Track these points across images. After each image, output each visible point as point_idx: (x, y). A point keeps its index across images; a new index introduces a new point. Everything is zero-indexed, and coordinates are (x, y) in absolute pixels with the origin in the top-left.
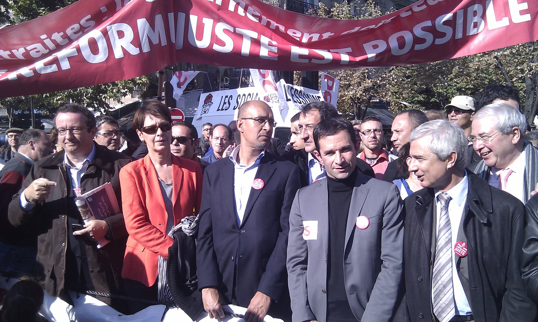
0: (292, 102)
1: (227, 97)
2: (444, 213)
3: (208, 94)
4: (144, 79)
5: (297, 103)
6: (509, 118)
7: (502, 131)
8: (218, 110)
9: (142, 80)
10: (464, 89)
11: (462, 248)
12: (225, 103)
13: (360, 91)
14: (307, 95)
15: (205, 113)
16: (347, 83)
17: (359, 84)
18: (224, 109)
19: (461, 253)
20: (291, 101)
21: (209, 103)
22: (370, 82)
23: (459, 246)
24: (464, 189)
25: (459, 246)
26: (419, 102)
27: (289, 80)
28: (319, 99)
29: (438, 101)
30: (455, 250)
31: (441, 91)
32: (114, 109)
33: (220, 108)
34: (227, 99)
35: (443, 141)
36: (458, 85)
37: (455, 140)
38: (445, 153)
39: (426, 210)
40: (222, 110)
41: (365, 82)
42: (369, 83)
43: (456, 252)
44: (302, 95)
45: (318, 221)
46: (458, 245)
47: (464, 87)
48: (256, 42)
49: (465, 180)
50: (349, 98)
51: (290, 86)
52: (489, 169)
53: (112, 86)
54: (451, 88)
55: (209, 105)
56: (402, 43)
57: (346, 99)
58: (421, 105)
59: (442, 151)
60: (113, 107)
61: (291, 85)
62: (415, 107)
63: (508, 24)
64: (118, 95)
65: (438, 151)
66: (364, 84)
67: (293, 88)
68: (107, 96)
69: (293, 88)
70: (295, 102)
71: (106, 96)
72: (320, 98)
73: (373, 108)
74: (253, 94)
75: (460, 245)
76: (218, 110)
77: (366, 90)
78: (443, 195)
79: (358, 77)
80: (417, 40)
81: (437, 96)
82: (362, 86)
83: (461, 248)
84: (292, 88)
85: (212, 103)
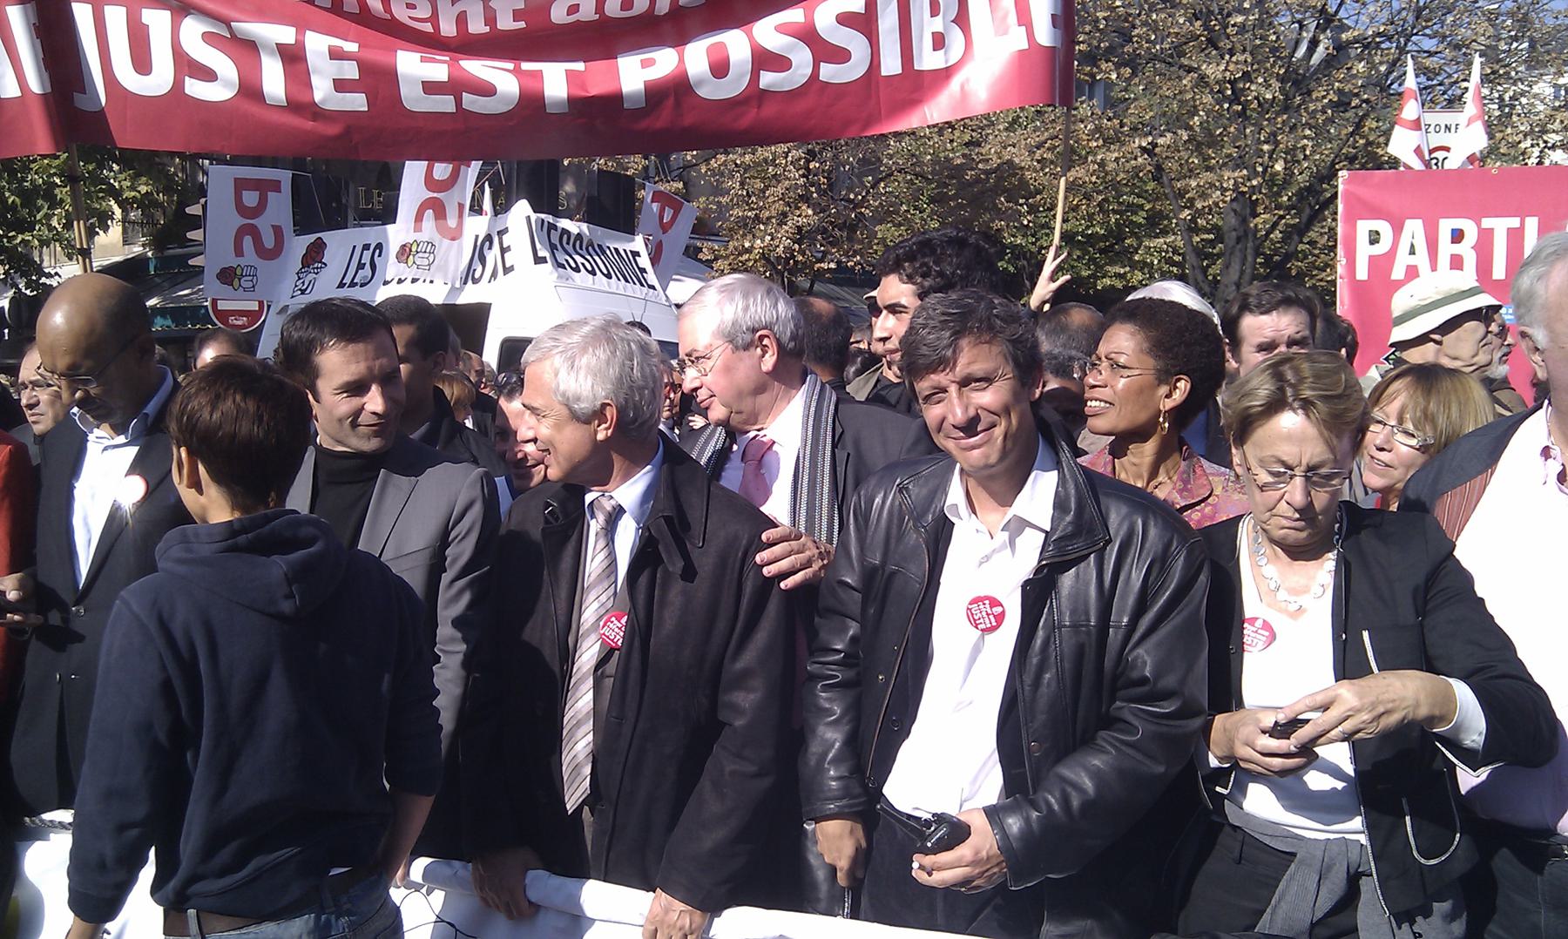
0: (549, 266)
1: (366, 247)
2: (602, 544)
3: (312, 238)
4: (146, 188)
5: (566, 269)
6: (746, 308)
7: (731, 342)
8: (341, 285)
9: (139, 189)
10: (1080, 238)
11: (988, 615)
12: (361, 266)
13: (784, 238)
14: (600, 246)
15: (302, 294)
16: (750, 214)
17: (783, 218)
18: (356, 284)
20: (547, 262)
21: (316, 265)
27: (545, 201)
28: (637, 258)
29: (1011, 269)
30: (970, 607)
31: (1019, 242)
32: (57, 277)
33: (347, 280)
34: (367, 255)
35: (582, 374)
37: (613, 372)
38: (584, 406)
39: (567, 538)
40: (353, 284)
41: (798, 213)
42: (809, 216)
44: (584, 248)
47: (1080, 230)
48: (293, 57)
50: (757, 257)
51: (546, 220)
52: (728, 439)
53: (46, 207)
55: (316, 271)
56: (720, 68)
57: (749, 260)
59: (578, 399)
60: (53, 272)
61: (549, 218)
64: (67, 236)
65: (568, 399)
66: (795, 218)
67: (555, 227)
68: (30, 238)
69: (556, 226)
70: (559, 267)
71: (27, 238)
72: (639, 256)
73: (842, 286)
76: (341, 285)
77: (801, 235)
79: (781, 199)
80: (764, 59)
81: (1009, 255)
82: (789, 223)
84: (552, 227)
85: (326, 265)
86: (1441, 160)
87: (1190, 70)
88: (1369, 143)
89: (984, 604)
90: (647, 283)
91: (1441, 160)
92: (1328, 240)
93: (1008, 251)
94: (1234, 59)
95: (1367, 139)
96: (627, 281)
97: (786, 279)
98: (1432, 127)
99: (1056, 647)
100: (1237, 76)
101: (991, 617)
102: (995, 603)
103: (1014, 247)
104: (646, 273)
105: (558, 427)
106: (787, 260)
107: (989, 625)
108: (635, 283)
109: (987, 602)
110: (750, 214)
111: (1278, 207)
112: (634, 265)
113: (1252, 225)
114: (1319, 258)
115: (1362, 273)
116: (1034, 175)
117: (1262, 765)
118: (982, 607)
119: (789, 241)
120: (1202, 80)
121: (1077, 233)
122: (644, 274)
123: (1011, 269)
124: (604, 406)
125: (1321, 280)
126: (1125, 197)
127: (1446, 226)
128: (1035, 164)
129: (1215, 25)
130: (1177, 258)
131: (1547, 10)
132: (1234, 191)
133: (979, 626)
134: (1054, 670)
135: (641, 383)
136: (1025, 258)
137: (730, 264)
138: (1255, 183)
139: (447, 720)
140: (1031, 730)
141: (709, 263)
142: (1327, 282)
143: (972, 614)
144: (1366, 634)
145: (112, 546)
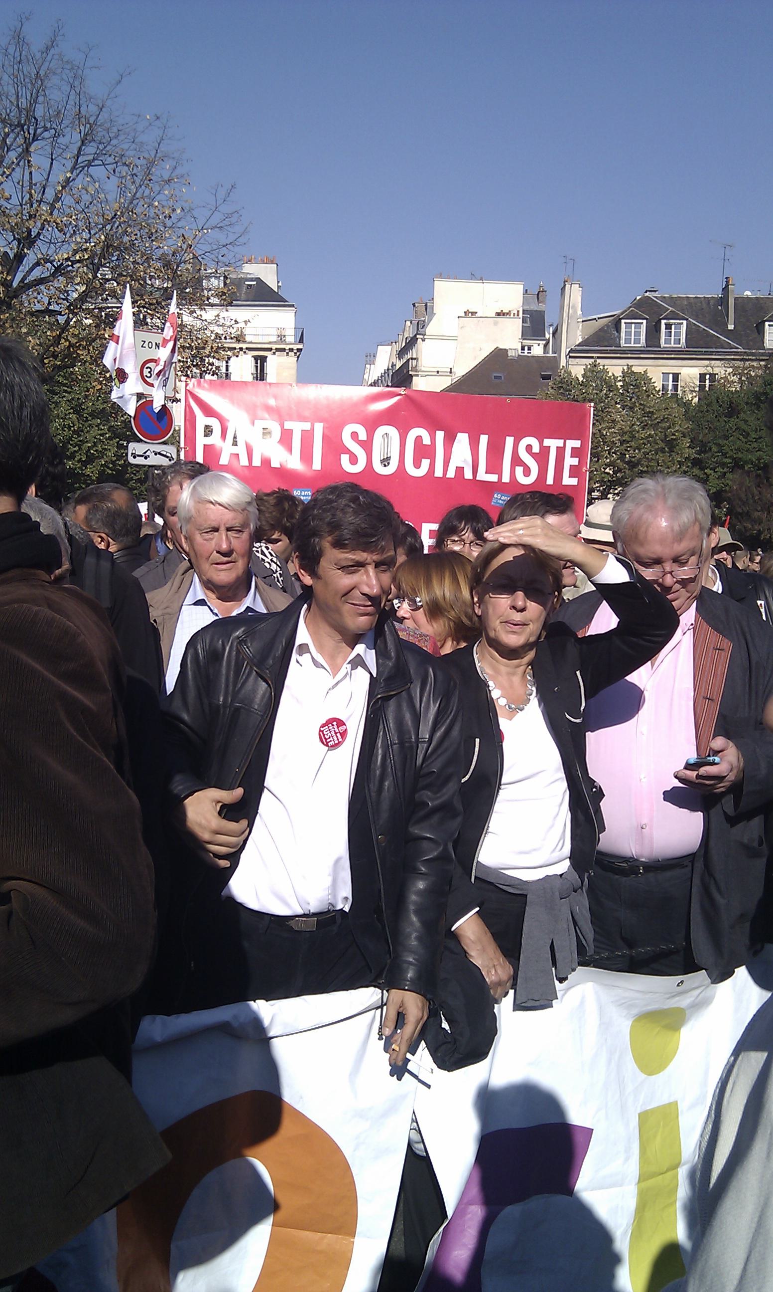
11: (336, 733)
19: (328, 741)
23: (333, 725)
25: (333, 725)
30: (322, 729)
43: (321, 733)
45: (423, 524)
46: (333, 723)
63: (496, 480)
74: (429, 1086)
75: (335, 726)
83: (335, 731)
98: (147, 343)
99: (391, 760)
101: (338, 735)
102: (340, 723)
107: (336, 742)
109: (335, 723)
118: (331, 728)
134: (391, 778)
139: (711, 1185)
140: (377, 827)
143: (324, 735)
145: (540, 772)
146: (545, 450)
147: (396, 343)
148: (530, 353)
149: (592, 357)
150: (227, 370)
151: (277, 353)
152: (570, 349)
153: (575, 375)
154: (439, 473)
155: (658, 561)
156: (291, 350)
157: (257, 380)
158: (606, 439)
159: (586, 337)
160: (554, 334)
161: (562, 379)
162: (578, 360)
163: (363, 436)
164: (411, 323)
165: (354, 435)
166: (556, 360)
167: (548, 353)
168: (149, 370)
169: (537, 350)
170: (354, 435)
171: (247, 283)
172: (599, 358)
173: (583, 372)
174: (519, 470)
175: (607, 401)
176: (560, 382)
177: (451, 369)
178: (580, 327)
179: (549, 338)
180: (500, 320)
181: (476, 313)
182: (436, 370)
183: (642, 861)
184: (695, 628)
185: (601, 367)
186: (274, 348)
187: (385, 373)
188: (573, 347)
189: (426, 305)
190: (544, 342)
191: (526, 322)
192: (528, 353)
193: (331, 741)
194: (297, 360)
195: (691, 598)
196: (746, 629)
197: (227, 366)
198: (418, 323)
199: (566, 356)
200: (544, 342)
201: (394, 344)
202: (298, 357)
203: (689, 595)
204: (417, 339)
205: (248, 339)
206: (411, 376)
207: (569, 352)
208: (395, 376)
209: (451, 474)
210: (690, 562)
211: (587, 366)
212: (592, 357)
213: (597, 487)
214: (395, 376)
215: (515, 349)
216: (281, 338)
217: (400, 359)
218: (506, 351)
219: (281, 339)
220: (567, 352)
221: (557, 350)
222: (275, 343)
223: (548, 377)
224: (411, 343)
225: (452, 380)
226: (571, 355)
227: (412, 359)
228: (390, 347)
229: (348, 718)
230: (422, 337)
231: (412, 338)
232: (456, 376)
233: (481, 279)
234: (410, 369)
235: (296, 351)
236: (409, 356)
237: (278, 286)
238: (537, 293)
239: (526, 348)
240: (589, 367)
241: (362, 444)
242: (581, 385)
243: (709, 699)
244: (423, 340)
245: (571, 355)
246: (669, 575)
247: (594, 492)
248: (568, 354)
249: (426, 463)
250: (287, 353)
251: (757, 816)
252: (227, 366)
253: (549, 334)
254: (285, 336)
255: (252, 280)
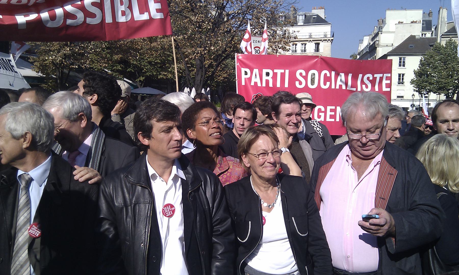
10: (153, 63)
11: (170, 211)
19: (166, 214)
22: (68, 49)
24: (45, 171)
25: (33, 227)
26: (118, 71)
29: (133, 71)
30: (29, 232)
31: (135, 63)
36: (148, 59)
41: (64, 49)
43: (163, 210)
49: (48, 161)
50: (50, 63)
54: (143, 61)
58: (120, 73)
62: (115, 75)
75: (170, 207)
77: (66, 56)
78: (25, 175)
81: (132, 67)
86: (257, 50)
87: (186, 17)
88: (235, 43)
89: (169, 207)
90: (14, 71)
91: (257, 50)
92: (220, 68)
93: (131, 65)
94: (200, 16)
95: (235, 42)
96: (7, 70)
97: (60, 70)
98: (255, 41)
100: (200, 21)
101: (171, 211)
102: (172, 206)
103: (133, 64)
104: (14, 67)
105: (7, 142)
106: (61, 64)
107: (170, 215)
108: (10, 71)
109: (170, 206)
110: (47, 48)
111: (211, 59)
112: (9, 65)
113: (204, 64)
114: (218, 73)
115: (243, 83)
116: (141, 44)
117: (93, 141)
119: (61, 58)
120: (191, 21)
121: (152, 62)
122: (13, 68)
123: (133, 71)
124: (26, 133)
125: (219, 79)
126: (166, 52)
127: (265, 71)
128: (142, 40)
129: (194, 5)
130: (181, 71)
131: (279, 11)
132: (200, 54)
133: (167, 215)
135: (43, 127)
136: (137, 68)
137: (40, 64)
138: (206, 52)
141: (32, 63)
142: (220, 80)
144: (293, 218)
146: (375, 79)
147: (371, 35)
148: (425, 36)
149: (449, 37)
150: (305, 48)
151: (324, 41)
152: (442, 34)
153: (442, 44)
154: (333, 87)
155: (359, 131)
156: (329, 40)
157: (316, 51)
158: (455, 69)
159: (449, 29)
160: (435, 29)
161: (436, 46)
162: (445, 38)
163: (304, 74)
164: (377, 27)
165: (301, 74)
166: (436, 39)
167: (433, 36)
168: (256, 50)
169: (428, 35)
170: (301, 74)
171: (313, 17)
172: (452, 37)
173: (445, 43)
174: (364, 86)
175: (455, 54)
176: (436, 47)
177: (392, 44)
178: (446, 26)
179: (433, 31)
180: (413, 24)
181: (403, 22)
182: (386, 45)
183: (350, 272)
184: (380, 163)
185: (454, 41)
186: (322, 40)
187: (366, 46)
188: (443, 34)
189: (383, 20)
190: (431, 32)
191: (424, 25)
192: (425, 36)
193: (167, 214)
194: (331, 44)
195: (378, 149)
196: (406, 165)
197: (305, 47)
198: (379, 27)
199: (440, 37)
200: (431, 32)
201: (370, 35)
202: (332, 42)
203: (377, 148)
204: (379, 33)
205: (298, 37)
206: (376, 47)
207: (442, 35)
208: (370, 48)
209: (338, 87)
210: (376, 132)
211: (447, 41)
212: (449, 37)
213: (452, 88)
214: (370, 48)
215: (419, 35)
216: (325, 36)
217: (372, 41)
218: (415, 36)
219: (325, 36)
220: (441, 35)
221: (437, 35)
222: (323, 38)
223: (432, 46)
224: (377, 35)
225: (393, 48)
226: (442, 36)
227: (377, 41)
228: (369, 37)
229: (175, 203)
230: (381, 32)
231: (377, 33)
232: (394, 47)
233: (405, 9)
234: (376, 44)
235: (331, 40)
236: (376, 40)
237: (325, 17)
238: (428, 13)
239: (424, 35)
240: (448, 41)
241: (304, 77)
242: (445, 48)
243: (382, 198)
244: (381, 34)
245: (442, 36)
246: (364, 137)
247: (450, 90)
248: (441, 36)
249: (328, 83)
250: (328, 41)
251: (415, 254)
252: (305, 47)
253: (433, 29)
254: (327, 35)
255: (315, 15)
